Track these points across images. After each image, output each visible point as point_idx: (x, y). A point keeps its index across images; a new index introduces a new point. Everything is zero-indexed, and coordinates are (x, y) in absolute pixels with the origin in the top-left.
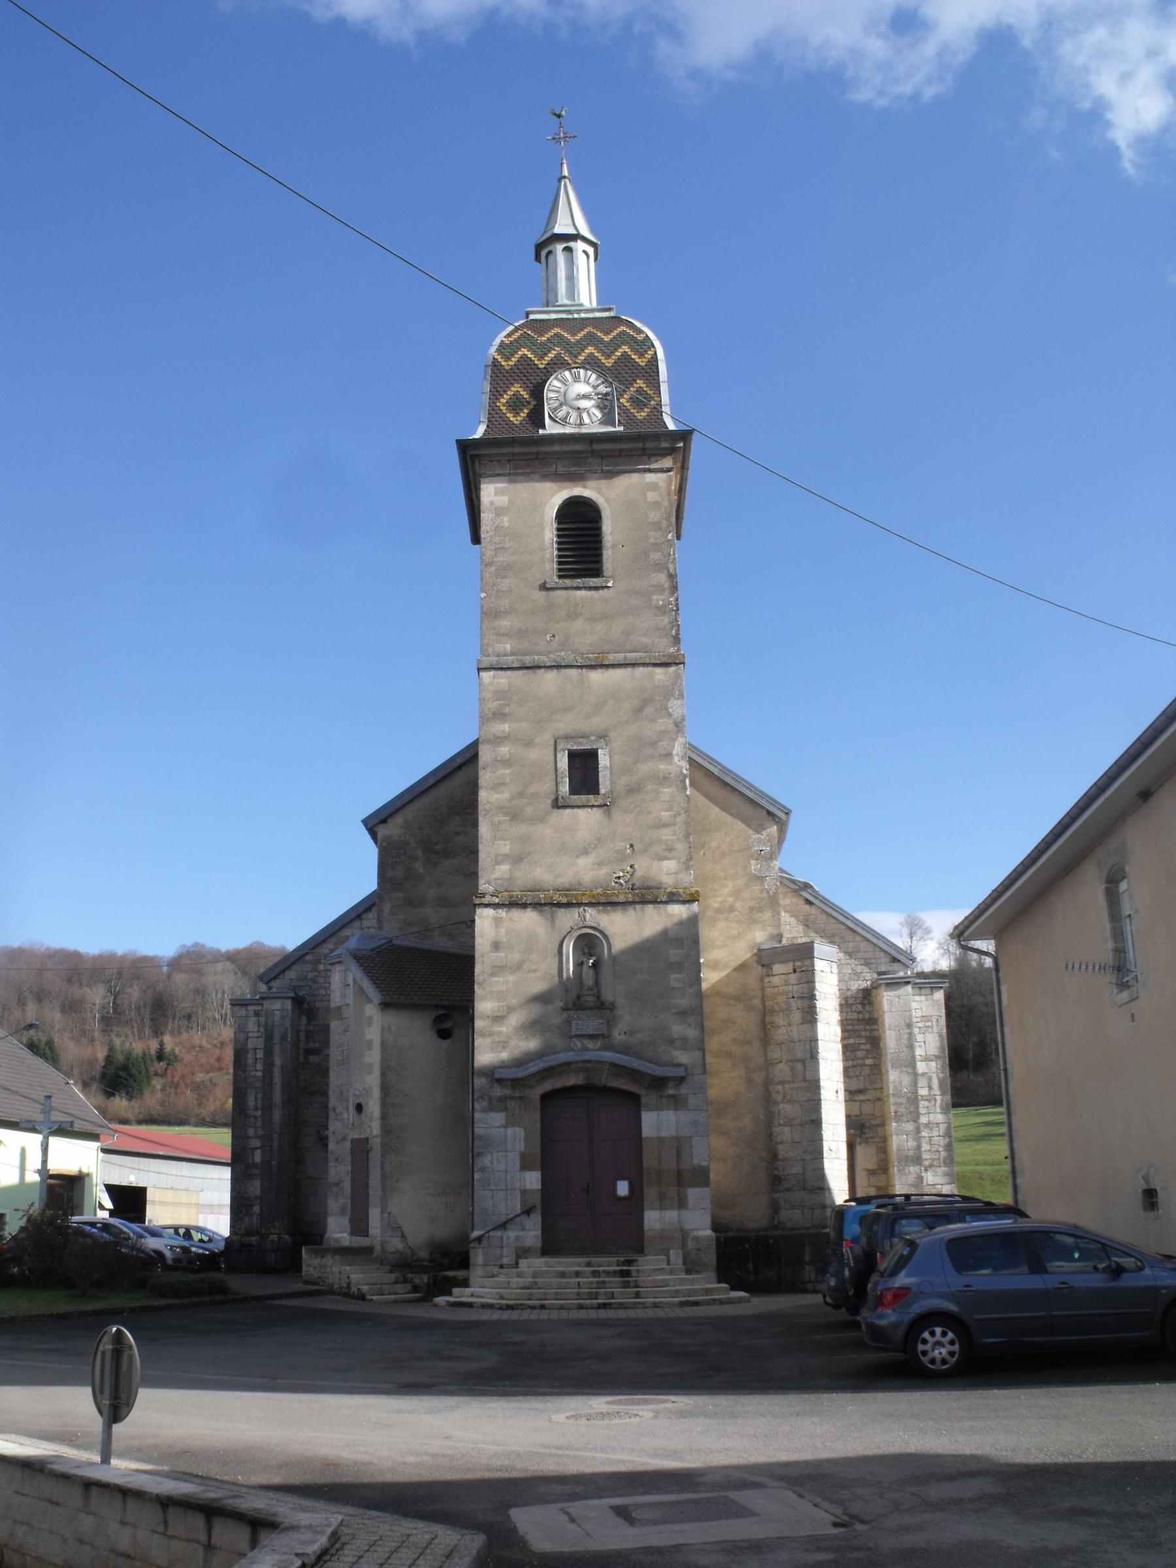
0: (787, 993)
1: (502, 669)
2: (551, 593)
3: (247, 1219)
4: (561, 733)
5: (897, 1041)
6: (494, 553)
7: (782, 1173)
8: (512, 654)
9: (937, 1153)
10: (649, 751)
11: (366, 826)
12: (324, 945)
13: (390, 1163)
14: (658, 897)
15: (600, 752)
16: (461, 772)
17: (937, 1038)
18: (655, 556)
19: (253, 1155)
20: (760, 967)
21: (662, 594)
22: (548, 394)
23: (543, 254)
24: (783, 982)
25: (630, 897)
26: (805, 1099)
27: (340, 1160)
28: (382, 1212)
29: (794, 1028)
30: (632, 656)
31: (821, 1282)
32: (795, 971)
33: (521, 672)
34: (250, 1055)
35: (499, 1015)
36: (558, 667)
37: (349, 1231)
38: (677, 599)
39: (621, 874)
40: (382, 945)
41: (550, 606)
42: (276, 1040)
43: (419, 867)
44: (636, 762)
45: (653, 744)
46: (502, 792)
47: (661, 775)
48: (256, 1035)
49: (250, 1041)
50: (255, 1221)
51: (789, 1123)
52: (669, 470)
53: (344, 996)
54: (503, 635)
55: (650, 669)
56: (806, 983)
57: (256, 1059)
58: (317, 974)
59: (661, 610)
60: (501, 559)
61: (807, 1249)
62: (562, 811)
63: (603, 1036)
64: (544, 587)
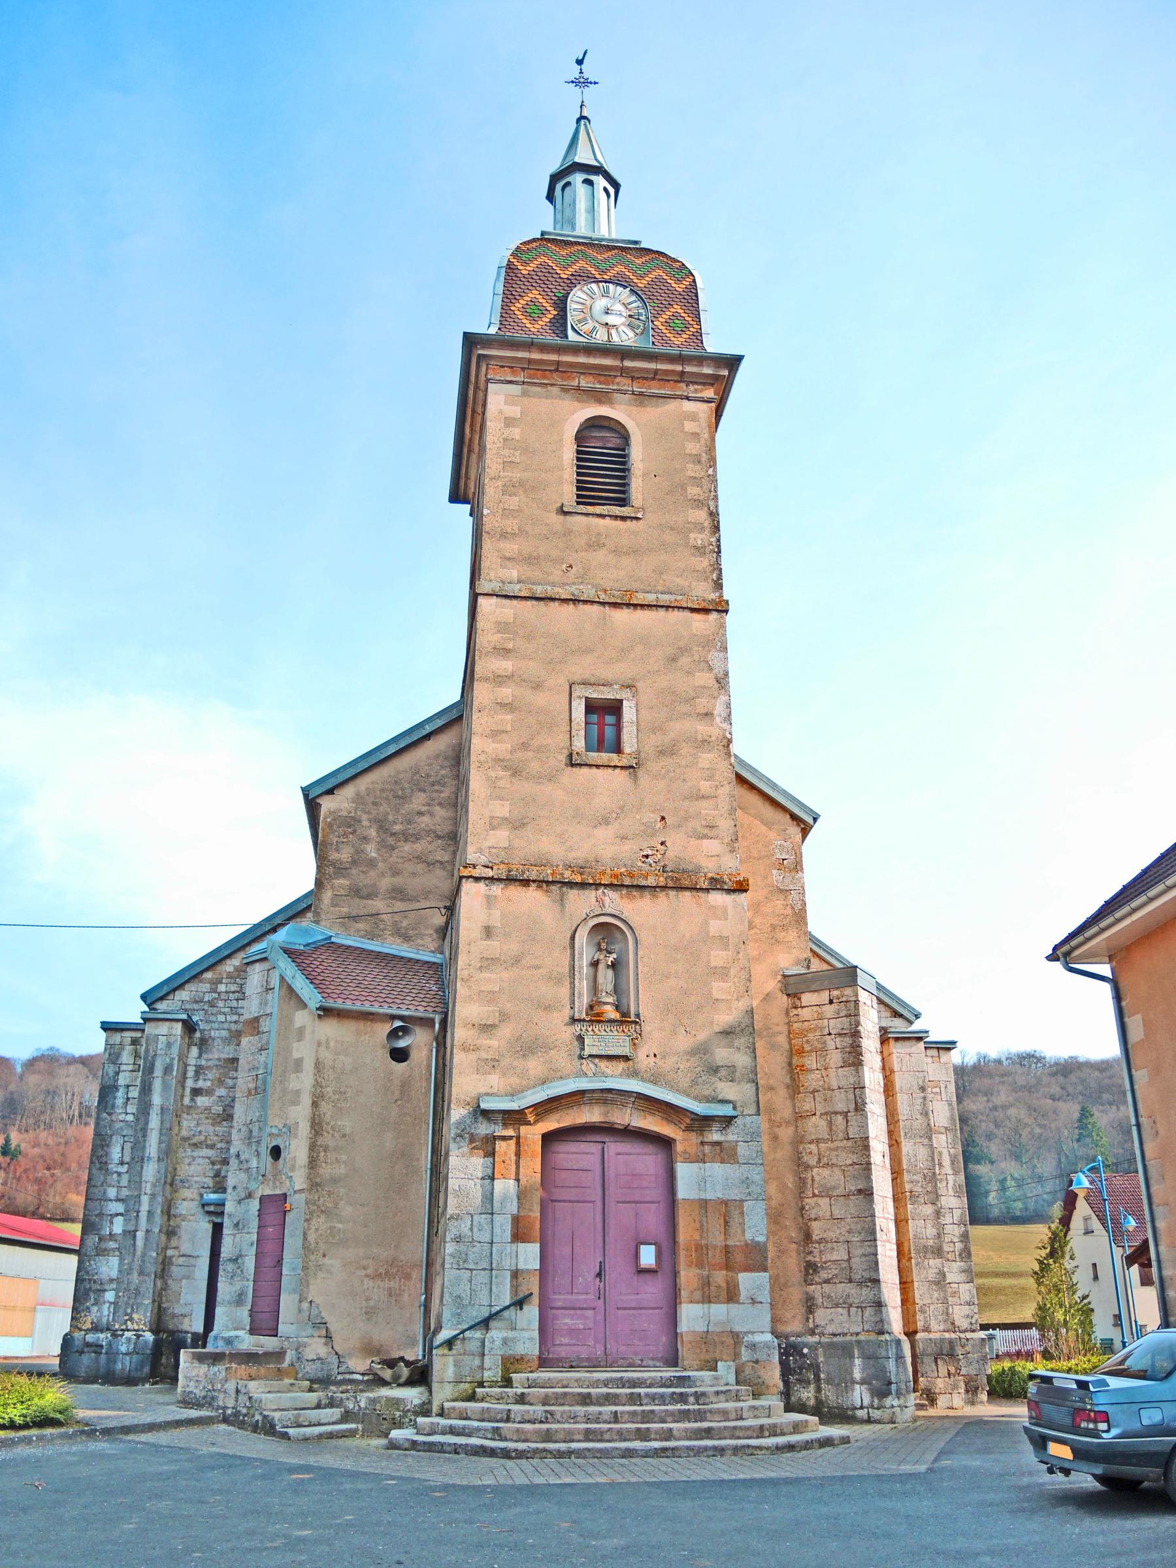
0: (822, 1029)
1: (506, 597)
2: (568, 518)
3: (95, 1309)
4: (577, 678)
5: (910, 1106)
6: (501, 466)
7: (818, 1259)
8: (519, 582)
9: (952, 1245)
10: (685, 708)
11: (306, 796)
12: (228, 962)
13: (317, 1230)
14: (697, 883)
15: (625, 703)
16: (429, 742)
17: (947, 1107)
18: (693, 491)
19: (112, 1223)
20: (785, 997)
21: (700, 533)
22: (571, 305)
23: (559, 186)
24: (815, 1015)
25: (662, 881)
26: (849, 1162)
27: (241, 1226)
28: (300, 1301)
29: (832, 1072)
30: (665, 599)
31: (878, 1408)
32: (831, 1002)
33: (530, 603)
34: (120, 1094)
35: (488, 1023)
36: (575, 601)
37: (248, 1327)
38: (719, 540)
39: (650, 852)
40: (319, 941)
41: (568, 532)
42: (158, 1072)
43: (371, 850)
44: (669, 719)
45: (690, 700)
46: (501, 742)
47: (700, 737)
48: (130, 1067)
49: (121, 1075)
50: (106, 1313)
51: (827, 1193)
52: (709, 401)
53: (263, 1003)
54: (509, 559)
55: (687, 614)
56: (846, 1016)
57: (128, 1099)
58: (216, 995)
59: (700, 550)
60: (510, 474)
61: (857, 1362)
62: (576, 770)
63: (626, 1058)
64: (562, 512)
